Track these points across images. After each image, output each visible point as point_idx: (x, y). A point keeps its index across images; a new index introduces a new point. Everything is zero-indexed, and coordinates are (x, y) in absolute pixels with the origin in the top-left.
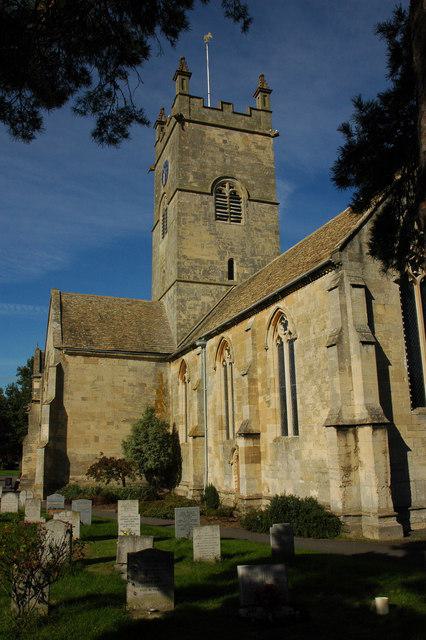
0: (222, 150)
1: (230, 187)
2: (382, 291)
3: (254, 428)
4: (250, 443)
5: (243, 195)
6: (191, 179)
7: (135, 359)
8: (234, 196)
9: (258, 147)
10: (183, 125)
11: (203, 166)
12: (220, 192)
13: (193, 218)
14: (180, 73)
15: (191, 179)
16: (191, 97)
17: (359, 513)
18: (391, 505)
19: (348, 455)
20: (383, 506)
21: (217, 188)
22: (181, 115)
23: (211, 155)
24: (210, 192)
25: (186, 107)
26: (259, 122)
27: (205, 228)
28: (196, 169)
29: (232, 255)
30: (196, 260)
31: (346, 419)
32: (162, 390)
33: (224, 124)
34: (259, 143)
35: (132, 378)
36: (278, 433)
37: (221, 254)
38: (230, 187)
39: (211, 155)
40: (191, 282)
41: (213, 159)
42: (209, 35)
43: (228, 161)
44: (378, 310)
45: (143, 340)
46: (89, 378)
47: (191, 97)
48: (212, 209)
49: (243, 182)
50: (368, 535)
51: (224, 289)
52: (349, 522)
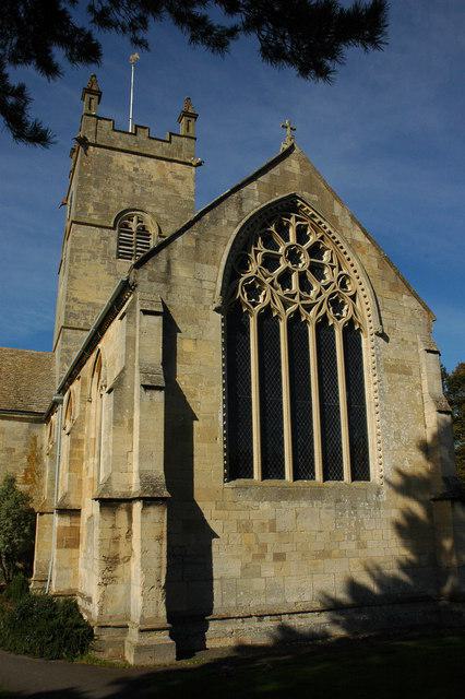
0: (131, 179)
1: (139, 221)
2: (194, 321)
3: (73, 503)
4: (66, 521)
6: (91, 210)
9: (177, 177)
10: (86, 149)
11: (106, 196)
12: (126, 226)
13: (88, 255)
14: (88, 91)
15: (91, 210)
16: (99, 118)
17: (124, 623)
18: (163, 613)
19: (116, 540)
20: (150, 614)
21: (121, 222)
22: (85, 139)
23: (117, 184)
24: (112, 225)
25: (93, 128)
26: (180, 150)
27: (103, 267)
30: (89, 304)
31: (117, 491)
32: (34, 458)
33: (136, 150)
34: (178, 173)
38: (139, 221)
39: (117, 184)
40: (82, 329)
42: (136, 55)
43: (138, 192)
44: (184, 345)
45: (18, 396)
47: (99, 118)
48: (113, 245)
50: (131, 659)
52: (105, 636)
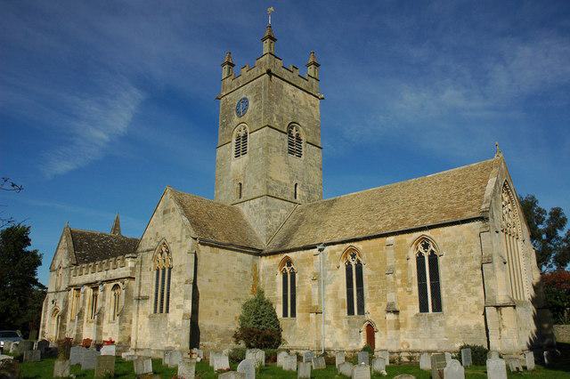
3: (398, 308)
5: (303, 137)
6: (275, 119)
7: (241, 251)
8: (299, 140)
11: (282, 111)
15: (275, 119)
27: (283, 158)
28: (277, 113)
29: (297, 181)
30: (278, 181)
35: (239, 266)
36: (417, 310)
37: (291, 178)
41: (287, 107)
42: (272, 9)
46: (214, 265)
49: (304, 128)
51: (293, 205)
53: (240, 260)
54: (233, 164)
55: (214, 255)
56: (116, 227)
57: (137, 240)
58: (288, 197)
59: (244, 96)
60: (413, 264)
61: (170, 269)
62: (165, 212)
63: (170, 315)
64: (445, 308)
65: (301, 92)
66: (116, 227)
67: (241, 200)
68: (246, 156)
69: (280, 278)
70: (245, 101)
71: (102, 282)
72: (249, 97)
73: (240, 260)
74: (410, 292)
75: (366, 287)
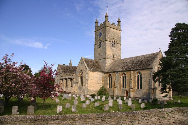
11: (110, 36)
35: (99, 76)
37: (112, 53)
46: (93, 76)
53: (99, 74)
54: (98, 49)
55: (93, 73)
56: (70, 63)
57: (76, 67)
58: (112, 58)
59: (100, 32)
60: (137, 77)
61: (83, 77)
62: (81, 63)
63: (83, 87)
64: (142, 88)
65: (115, 30)
66: (70, 63)
67: (100, 59)
68: (101, 48)
69: (108, 79)
70: (101, 33)
71: (68, 79)
72: (102, 32)
73: (99, 74)
74: (136, 84)
75: (126, 82)
